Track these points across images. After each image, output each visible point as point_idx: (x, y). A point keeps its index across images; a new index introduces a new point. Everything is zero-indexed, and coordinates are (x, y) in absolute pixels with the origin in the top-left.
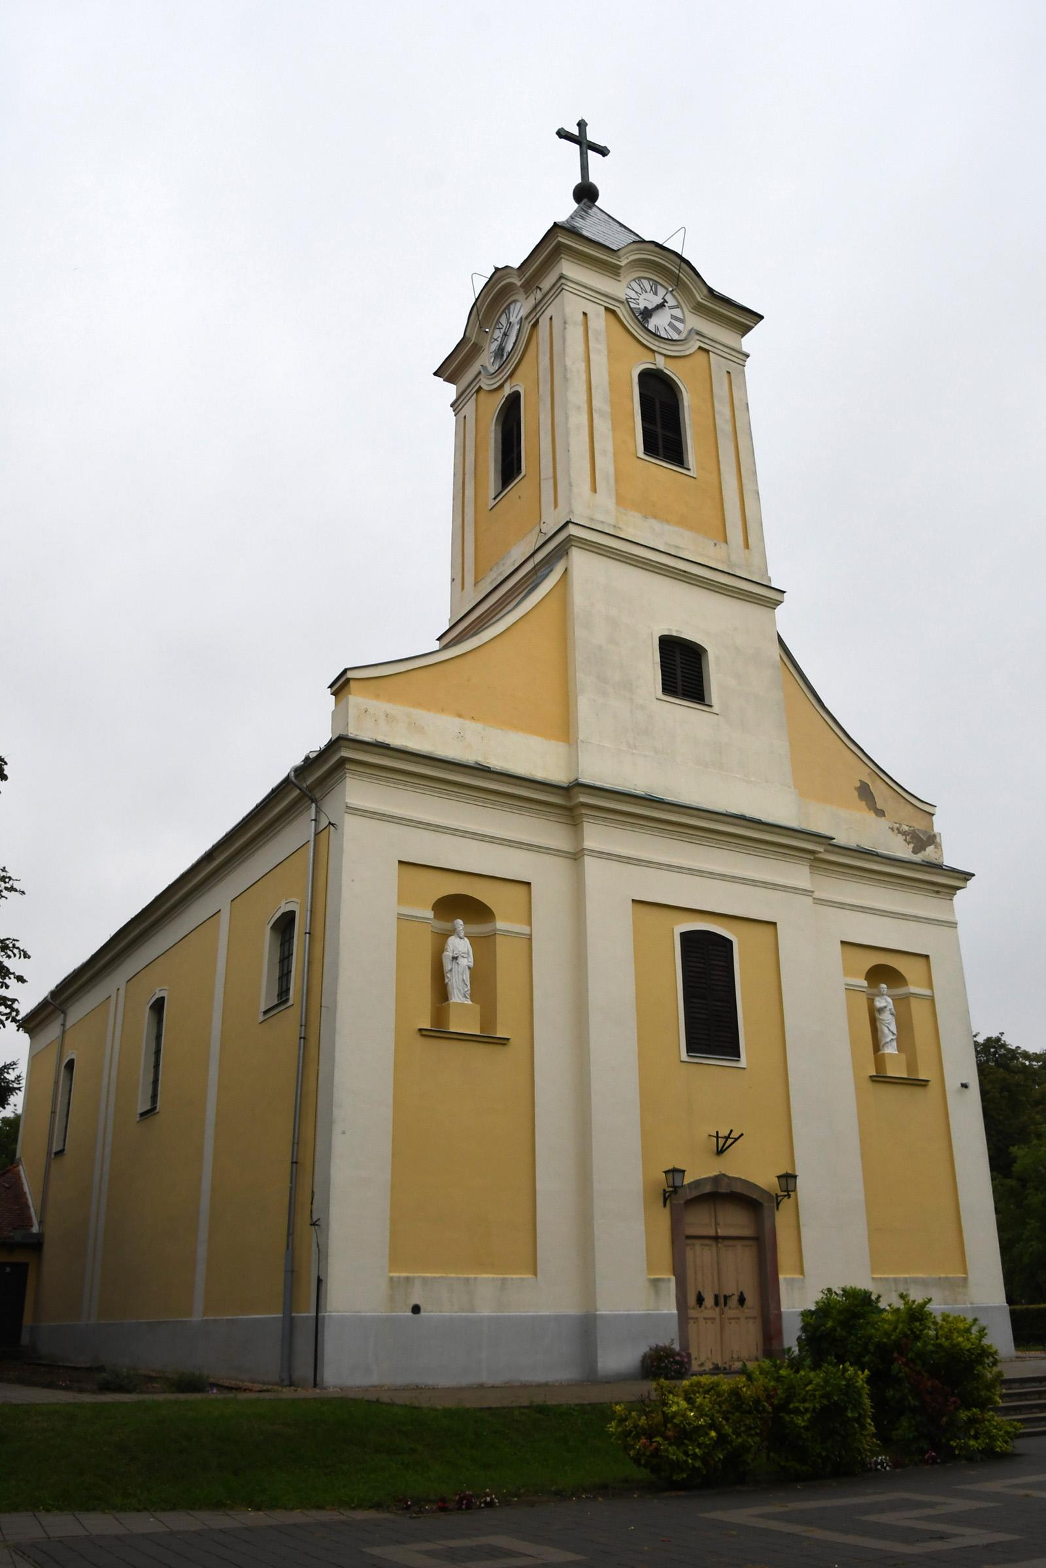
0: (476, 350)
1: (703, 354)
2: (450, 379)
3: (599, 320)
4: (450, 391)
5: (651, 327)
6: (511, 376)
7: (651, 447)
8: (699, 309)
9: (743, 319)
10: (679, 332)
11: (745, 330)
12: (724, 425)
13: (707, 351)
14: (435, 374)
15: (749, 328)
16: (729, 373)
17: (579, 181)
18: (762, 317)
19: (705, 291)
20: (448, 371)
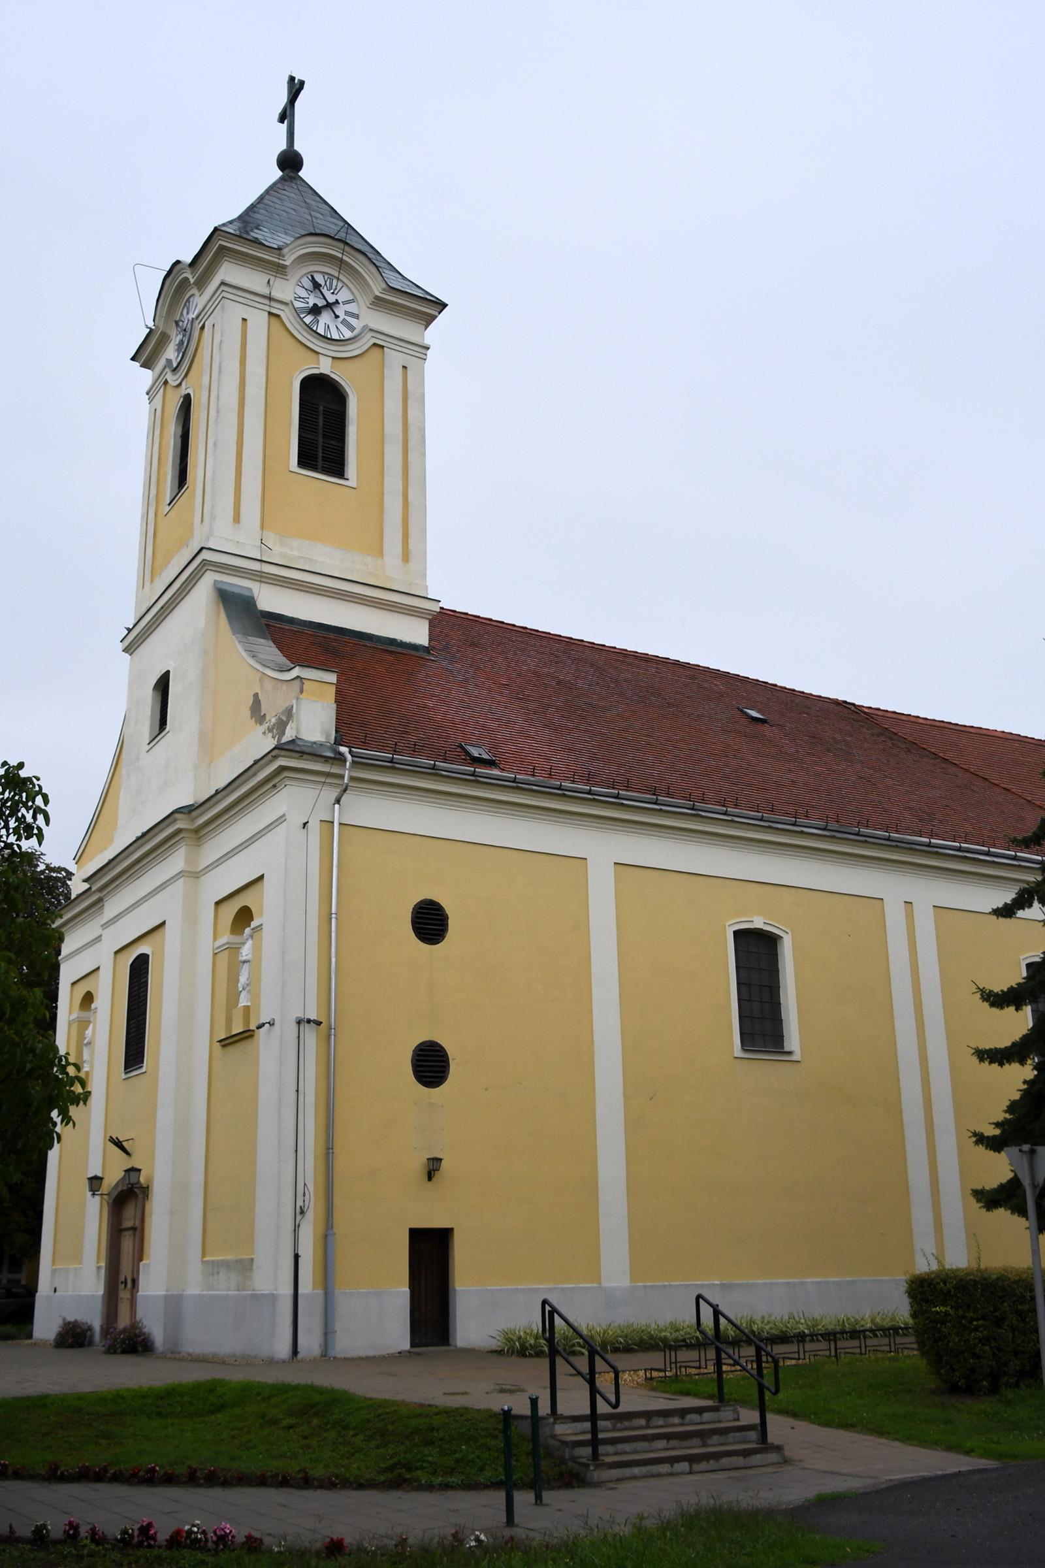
0: (164, 339)
1: (376, 351)
2: (146, 365)
3: (258, 320)
4: (146, 377)
5: (321, 331)
6: (186, 376)
7: (307, 459)
8: (379, 303)
9: (427, 308)
10: (352, 328)
11: (429, 320)
12: (393, 428)
13: (383, 347)
14: (133, 359)
15: (434, 318)
16: (405, 367)
17: (283, 146)
18: (445, 305)
19: (384, 286)
20: (145, 355)
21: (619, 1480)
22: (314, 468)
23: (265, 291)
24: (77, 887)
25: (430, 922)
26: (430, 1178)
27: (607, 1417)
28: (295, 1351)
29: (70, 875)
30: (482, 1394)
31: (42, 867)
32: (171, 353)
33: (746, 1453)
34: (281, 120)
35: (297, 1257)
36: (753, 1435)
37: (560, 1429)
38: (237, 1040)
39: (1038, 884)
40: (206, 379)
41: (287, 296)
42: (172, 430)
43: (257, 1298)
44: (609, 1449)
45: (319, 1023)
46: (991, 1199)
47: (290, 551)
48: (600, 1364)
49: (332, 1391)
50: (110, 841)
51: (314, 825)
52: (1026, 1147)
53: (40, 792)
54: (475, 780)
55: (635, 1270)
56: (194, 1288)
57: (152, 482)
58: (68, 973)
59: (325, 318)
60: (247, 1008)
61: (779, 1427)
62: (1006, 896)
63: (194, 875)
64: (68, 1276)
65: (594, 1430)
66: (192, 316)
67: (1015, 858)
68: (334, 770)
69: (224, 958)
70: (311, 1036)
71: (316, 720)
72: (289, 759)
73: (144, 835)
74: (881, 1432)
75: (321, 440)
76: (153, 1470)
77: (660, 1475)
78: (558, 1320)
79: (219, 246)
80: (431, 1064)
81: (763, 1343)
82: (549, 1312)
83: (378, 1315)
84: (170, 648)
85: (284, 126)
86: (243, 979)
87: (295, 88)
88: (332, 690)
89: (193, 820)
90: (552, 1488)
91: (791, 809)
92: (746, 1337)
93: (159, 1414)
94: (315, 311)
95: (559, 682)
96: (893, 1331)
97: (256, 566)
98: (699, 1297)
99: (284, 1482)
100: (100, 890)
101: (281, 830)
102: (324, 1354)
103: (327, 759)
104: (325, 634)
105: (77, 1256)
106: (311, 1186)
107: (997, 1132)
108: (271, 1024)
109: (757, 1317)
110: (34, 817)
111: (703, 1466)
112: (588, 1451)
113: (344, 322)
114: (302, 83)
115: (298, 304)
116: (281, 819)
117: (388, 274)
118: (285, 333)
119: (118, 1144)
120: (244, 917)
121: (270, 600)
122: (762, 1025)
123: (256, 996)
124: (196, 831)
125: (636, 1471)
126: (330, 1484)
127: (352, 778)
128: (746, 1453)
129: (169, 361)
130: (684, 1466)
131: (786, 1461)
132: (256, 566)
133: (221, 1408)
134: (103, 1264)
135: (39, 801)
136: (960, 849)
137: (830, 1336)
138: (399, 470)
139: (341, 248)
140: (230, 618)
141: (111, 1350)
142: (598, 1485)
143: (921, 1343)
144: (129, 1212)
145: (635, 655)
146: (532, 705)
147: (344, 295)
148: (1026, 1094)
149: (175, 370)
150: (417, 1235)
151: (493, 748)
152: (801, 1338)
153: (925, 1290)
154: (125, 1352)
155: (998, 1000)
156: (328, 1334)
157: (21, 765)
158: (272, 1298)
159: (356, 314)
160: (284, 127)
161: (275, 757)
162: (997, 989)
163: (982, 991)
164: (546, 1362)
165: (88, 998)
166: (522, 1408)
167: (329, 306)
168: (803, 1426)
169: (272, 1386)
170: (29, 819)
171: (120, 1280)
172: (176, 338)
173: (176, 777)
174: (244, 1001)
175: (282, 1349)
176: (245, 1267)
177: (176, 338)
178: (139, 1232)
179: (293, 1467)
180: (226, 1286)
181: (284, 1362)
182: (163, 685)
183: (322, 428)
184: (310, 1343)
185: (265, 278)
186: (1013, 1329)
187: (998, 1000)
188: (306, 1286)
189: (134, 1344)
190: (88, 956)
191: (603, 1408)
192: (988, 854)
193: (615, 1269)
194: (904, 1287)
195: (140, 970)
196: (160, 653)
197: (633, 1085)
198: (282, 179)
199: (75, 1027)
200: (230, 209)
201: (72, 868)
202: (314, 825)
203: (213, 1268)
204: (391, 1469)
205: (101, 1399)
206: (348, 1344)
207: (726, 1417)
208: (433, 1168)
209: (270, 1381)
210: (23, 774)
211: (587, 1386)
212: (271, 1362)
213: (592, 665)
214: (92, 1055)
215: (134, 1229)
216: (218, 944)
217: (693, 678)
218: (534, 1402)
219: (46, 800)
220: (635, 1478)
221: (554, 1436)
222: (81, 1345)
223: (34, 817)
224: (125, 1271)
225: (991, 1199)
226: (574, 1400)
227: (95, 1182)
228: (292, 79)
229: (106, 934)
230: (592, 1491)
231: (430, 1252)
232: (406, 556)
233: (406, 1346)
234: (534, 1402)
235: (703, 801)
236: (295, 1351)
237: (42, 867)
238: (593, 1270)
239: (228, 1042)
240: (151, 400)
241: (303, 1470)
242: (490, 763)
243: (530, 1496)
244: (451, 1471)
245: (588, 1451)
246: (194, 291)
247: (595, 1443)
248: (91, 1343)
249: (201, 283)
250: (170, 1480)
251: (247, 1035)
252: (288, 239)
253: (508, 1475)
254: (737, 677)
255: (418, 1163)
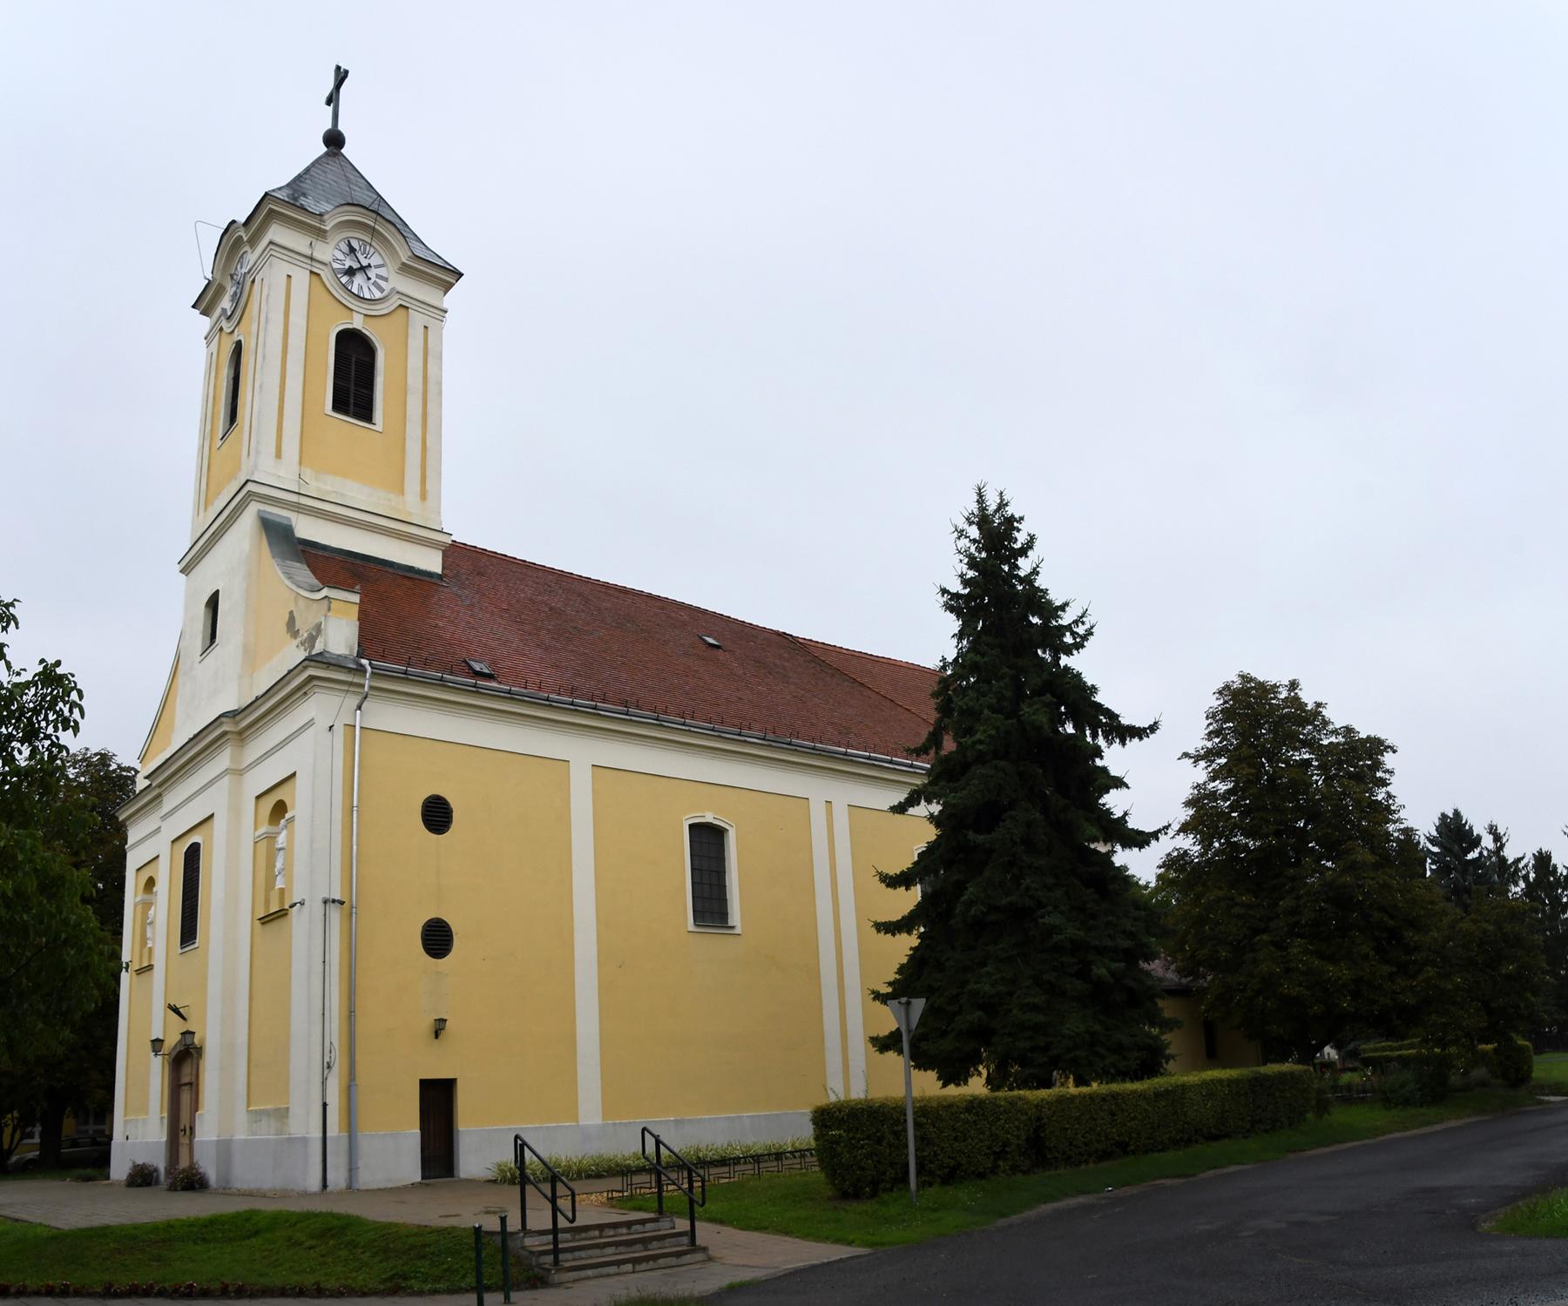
1: (402, 311)
2: (205, 313)
3: (301, 277)
4: (205, 323)
5: (355, 290)
7: (340, 404)
8: (405, 269)
9: (446, 276)
10: (382, 290)
11: (448, 287)
12: (414, 380)
15: (452, 285)
17: (329, 126)
18: (461, 275)
20: (205, 303)
21: (574, 1281)
22: (346, 413)
23: (308, 252)
24: (141, 784)
25: (437, 815)
26: (437, 1036)
27: (565, 1230)
28: (325, 1185)
29: (137, 772)
30: (470, 1214)
31: (114, 767)
32: (226, 303)
33: (678, 1254)
34: (329, 102)
35: (325, 1105)
36: (685, 1240)
37: (528, 1242)
38: (274, 917)
39: (925, 785)
40: (255, 327)
41: (326, 258)
42: (226, 372)
43: (291, 1140)
44: (569, 1256)
45: (342, 903)
46: (885, 1044)
47: (324, 485)
48: (561, 1190)
49: (348, 1216)
50: (169, 743)
51: (339, 728)
52: (904, 1000)
53: (75, 688)
54: (477, 691)
55: (607, 1111)
56: (241, 1135)
57: (208, 418)
58: (133, 860)
59: (359, 279)
60: (282, 890)
61: (705, 1232)
62: (900, 796)
63: (238, 772)
64: (137, 1129)
65: (556, 1242)
66: (245, 270)
67: (911, 766)
68: (356, 680)
69: (263, 845)
70: (335, 914)
71: (341, 636)
72: (318, 669)
73: (196, 736)
74: (787, 1233)
75: (352, 388)
76: (191, 1286)
77: (609, 1275)
78: (527, 1153)
79: (268, 210)
80: (437, 939)
81: (692, 1166)
82: (520, 1146)
83: (395, 1154)
84: (220, 570)
85: (330, 108)
86: (279, 865)
87: (341, 76)
88: (354, 611)
89: (237, 723)
90: (519, 1290)
91: (736, 721)
92: (680, 1164)
93: (204, 1239)
94: (351, 272)
95: (551, 609)
96: (799, 1153)
97: (294, 498)
98: (644, 1130)
99: (301, 1293)
100: (160, 786)
101: (311, 731)
102: (349, 1187)
103: (350, 670)
104: (351, 560)
105: (144, 1108)
106: (336, 1044)
107: (890, 990)
108: (302, 903)
109: (703, 1146)
110: (71, 711)
111: (644, 1266)
112: (550, 1258)
113: (375, 284)
114: (346, 72)
115: (336, 266)
116: (311, 723)
117: (414, 244)
118: (322, 290)
119: (176, 1011)
120: (280, 809)
121: (307, 529)
122: (710, 904)
123: (289, 880)
124: (240, 733)
125: (590, 1272)
126: (338, 1294)
127: (371, 688)
128: (678, 1254)
129: (224, 310)
130: (629, 1267)
131: (710, 1259)
132: (294, 498)
133: (256, 1233)
134: (165, 1115)
135: (74, 696)
136: (869, 758)
137: (757, 1159)
138: (419, 419)
139: (374, 218)
140: (270, 544)
141: (173, 1188)
142: (558, 1285)
143: (821, 1160)
144: (187, 1070)
145: (615, 588)
146: (527, 627)
147: (375, 260)
148: (911, 958)
149: (229, 318)
150: (425, 1084)
151: (493, 663)
152: (737, 1161)
153: (824, 1118)
154: (184, 1189)
155: (893, 881)
156: (352, 1169)
157: (58, 663)
158: (305, 1141)
159: (386, 276)
160: (330, 108)
161: (306, 668)
162: (891, 873)
163: (880, 874)
164: (518, 1188)
165: (151, 883)
166: (492, 1224)
167: (363, 269)
168: (728, 1232)
169: (299, 1214)
170: (67, 713)
171: (179, 1128)
172: (230, 290)
173: (223, 687)
174: (279, 884)
175: (314, 1184)
176: (282, 1114)
177: (230, 290)
178: (194, 1086)
179: (309, 1281)
180: (267, 1132)
181: (315, 1194)
182: (213, 603)
183: (354, 377)
184: (337, 1178)
185: (308, 240)
186: (890, 1146)
187: (893, 881)
188: (332, 1131)
189: (192, 1182)
190: (150, 845)
191: (562, 1223)
192: (891, 762)
193: (590, 1111)
194: (809, 1117)
195: (192, 857)
196: (212, 574)
197: (606, 955)
198: (326, 154)
199: (139, 908)
200: (279, 177)
201: (138, 767)
202: (339, 728)
203: (256, 1116)
204: (391, 1278)
205: (154, 1228)
206: (370, 1177)
207: (664, 1227)
208: (439, 1028)
209: (298, 1210)
210: (59, 671)
211: (549, 1206)
212: (305, 1194)
213: (579, 595)
214: (154, 933)
215: (190, 1084)
216: (259, 833)
217: (662, 608)
218: (503, 1220)
219: (81, 696)
220: (588, 1278)
221: (523, 1248)
222: (149, 1184)
223: (71, 711)
224: (184, 1121)
225: (885, 1044)
226: (540, 1218)
227: (157, 1044)
228: (338, 68)
229: (165, 825)
230: (552, 1291)
231: (438, 1099)
232: (423, 496)
233: (418, 1178)
234: (503, 1220)
235: (666, 713)
236: (325, 1185)
237: (114, 767)
238: (572, 1111)
239: (267, 920)
240: (208, 345)
241: (317, 1283)
242: (490, 677)
243: (500, 1297)
244: (438, 1279)
245: (550, 1258)
246: (247, 248)
247: (556, 1251)
248: (157, 1182)
249: (253, 241)
250: (205, 1294)
251: (282, 914)
252: (329, 207)
253: (479, 1281)
254: (698, 609)
255: (427, 1024)
